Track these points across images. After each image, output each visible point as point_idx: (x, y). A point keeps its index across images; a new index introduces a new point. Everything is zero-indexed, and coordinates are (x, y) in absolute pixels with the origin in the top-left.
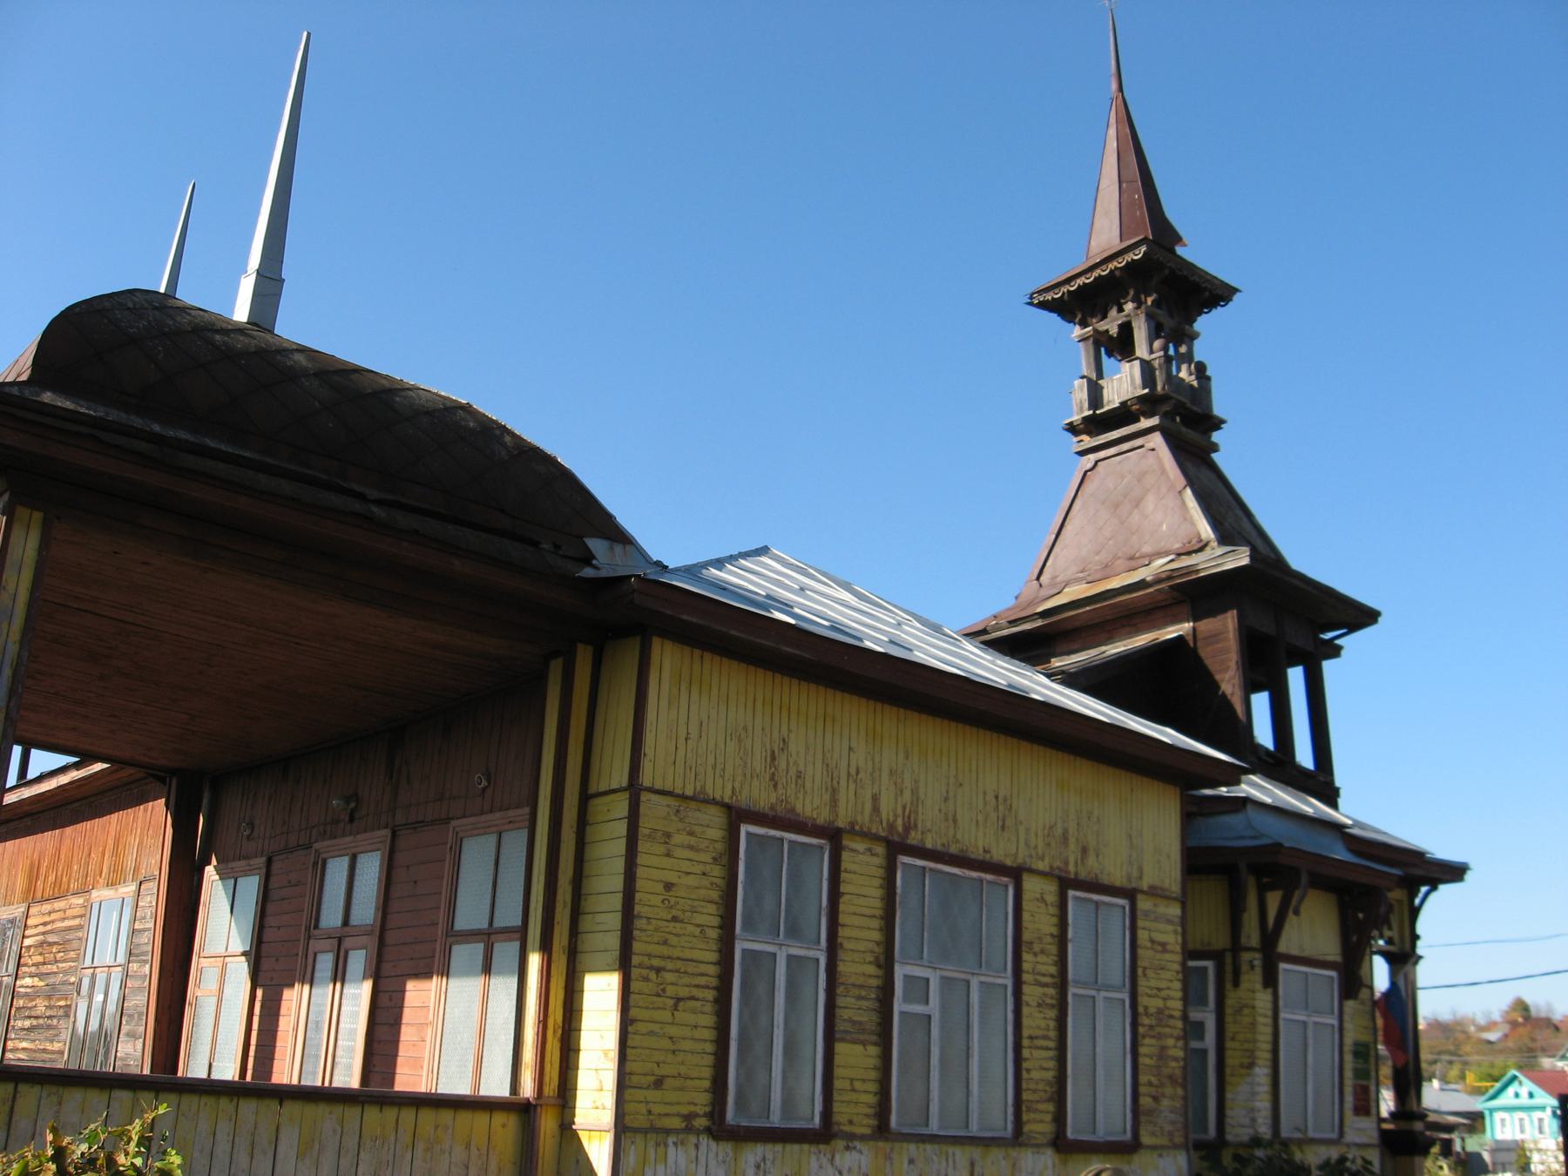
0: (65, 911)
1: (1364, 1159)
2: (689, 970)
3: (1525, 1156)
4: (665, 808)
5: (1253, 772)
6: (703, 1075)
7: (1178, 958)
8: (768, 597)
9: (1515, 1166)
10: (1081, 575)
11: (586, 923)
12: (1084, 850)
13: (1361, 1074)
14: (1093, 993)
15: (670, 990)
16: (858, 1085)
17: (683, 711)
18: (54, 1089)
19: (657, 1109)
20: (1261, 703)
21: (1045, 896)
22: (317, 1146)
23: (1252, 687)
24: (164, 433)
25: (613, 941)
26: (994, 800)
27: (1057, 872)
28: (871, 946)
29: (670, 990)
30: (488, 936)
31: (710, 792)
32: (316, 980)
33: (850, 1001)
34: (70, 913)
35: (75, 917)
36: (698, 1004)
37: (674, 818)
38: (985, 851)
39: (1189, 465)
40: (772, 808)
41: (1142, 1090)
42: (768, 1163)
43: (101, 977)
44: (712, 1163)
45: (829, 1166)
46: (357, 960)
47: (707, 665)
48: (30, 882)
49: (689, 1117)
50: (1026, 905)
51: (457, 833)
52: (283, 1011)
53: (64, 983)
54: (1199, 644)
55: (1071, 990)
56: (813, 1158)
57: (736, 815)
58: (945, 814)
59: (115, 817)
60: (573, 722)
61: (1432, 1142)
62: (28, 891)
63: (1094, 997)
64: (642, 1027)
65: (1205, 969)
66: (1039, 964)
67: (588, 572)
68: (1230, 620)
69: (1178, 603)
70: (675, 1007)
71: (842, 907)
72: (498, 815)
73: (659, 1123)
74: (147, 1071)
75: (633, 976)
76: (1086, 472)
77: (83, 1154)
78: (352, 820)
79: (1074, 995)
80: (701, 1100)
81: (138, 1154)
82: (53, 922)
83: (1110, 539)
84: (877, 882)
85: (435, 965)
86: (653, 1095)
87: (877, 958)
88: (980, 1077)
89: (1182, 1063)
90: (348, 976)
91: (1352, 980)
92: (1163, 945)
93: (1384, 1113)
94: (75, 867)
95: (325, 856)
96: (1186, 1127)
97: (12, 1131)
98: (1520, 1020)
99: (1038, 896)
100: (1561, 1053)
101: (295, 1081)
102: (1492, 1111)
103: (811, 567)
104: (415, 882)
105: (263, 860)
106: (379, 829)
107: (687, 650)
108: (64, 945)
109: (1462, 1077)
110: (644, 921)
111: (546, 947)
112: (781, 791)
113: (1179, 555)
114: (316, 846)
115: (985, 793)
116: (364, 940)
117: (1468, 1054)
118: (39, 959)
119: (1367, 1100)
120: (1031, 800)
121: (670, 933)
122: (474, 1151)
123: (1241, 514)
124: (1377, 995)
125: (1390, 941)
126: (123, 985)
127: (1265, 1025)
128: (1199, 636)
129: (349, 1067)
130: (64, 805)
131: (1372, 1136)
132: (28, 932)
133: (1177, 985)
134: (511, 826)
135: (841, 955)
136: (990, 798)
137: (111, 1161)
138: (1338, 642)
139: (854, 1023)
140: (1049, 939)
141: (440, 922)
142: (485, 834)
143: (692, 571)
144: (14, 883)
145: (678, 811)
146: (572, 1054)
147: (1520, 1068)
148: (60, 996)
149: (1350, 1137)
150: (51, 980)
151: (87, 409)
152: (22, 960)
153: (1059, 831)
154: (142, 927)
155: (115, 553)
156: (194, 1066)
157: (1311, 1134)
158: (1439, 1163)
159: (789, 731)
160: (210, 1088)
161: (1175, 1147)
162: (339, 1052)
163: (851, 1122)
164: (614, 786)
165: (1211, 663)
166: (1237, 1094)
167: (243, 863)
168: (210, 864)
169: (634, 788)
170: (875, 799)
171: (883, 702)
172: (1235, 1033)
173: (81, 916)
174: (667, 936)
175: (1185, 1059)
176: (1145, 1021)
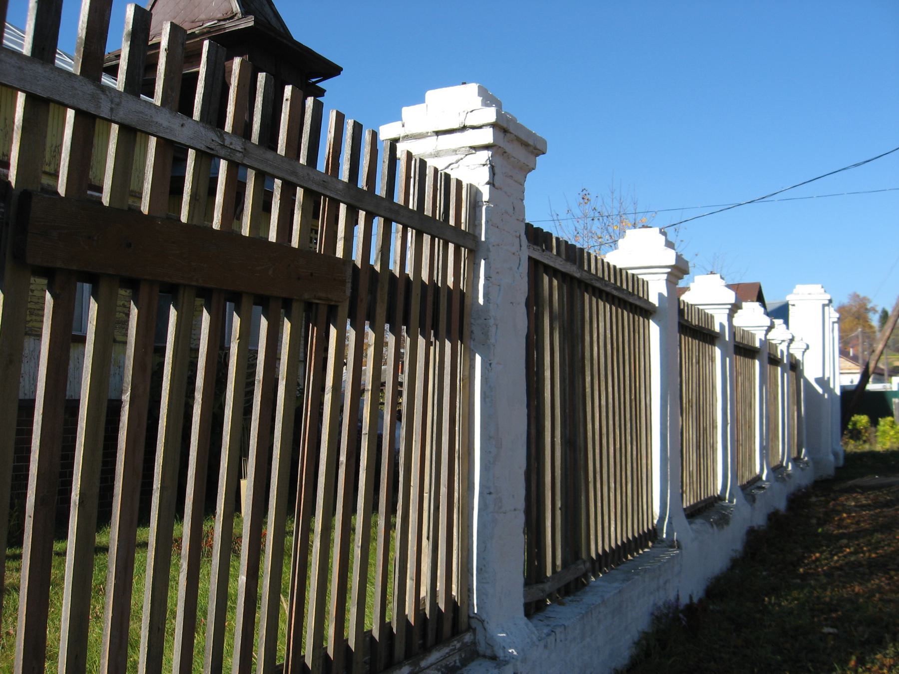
83: (182, 10)
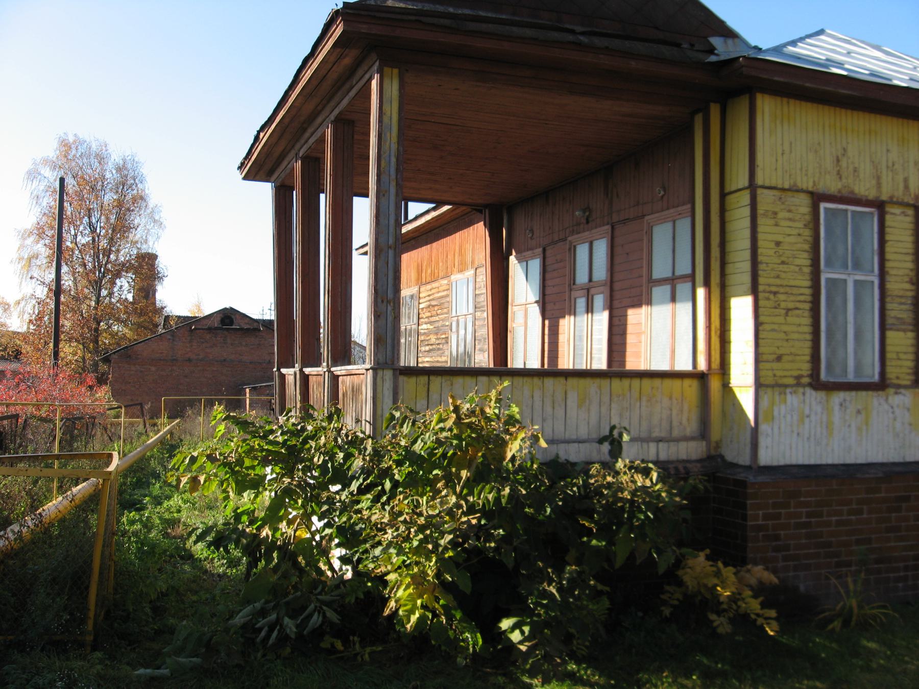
0: (438, 288)
2: (794, 292)
4: (773, 197)
8: (827, 60)
11: (730, 269)
15: (783, 305)
16: (902, 356)
18: (448, 378)
19: (779, 373)
22: (587, 401)
24: (455, 12)
25: (747, 278)
29: (783, 305)
30: (672, 281)
32: (577, 313)
33: (894, 306)
34: (441, 289)
35: (444, 291)
37: (778, 202)
40: (839, 191)
46: (599, 300)
48: (418, 275)
49: (798, 378)
51: (649, 223)
52: (561, 331)
53: (443, 326)
57: (817, 198)
59: (457, 235)
62: (418, 279)
64: (766, 327)
67: (713, 58)
70: (787, 315)
72: (672, 211)
73: (781, 381)
74: (492, 366)
77: (468, 409)
78: (588, 222)
80: (805, 368)
81: (496, 407)
85: (642, 299)
86: (775, 365)
87: (911, 279)
90: (595, 309)
94: (441, 264)
95: (574, 244)
101: (571, 367)
103: (854, 39)
104: (627, 254)
105: (541, 249)
106: (604, 226)
107: (779, 99)
110: (764, 265)
111: (707, 284)
112: (844, 181)
114: (569, 239)
116: (602, 288)
118: (429, 314)
121: (780, 271)
126: (474, 325)
129: (600, 359)
130: (430, 231)
134: (680, 216)
135: (888, 278)
137: (483, 411)
139: (898, 319)
141: (644, 274)
142: (665, 222)
143: (777, 50)
144: (410, 276)
145: (780, 198)
148: (442, 334)
150: (436, 325)
151: (412, 6)
152: (420, 316)
154: (480, 292)
155: (440, 86)
156: (516, 361)
160: (525, 373)
162: (594, 352)
164: (740, 186)
167: (530, 252)
168: (512, 255)
169: (752, 187)
170: (906, 180)
173: (447, 290)
174: (780, 273)
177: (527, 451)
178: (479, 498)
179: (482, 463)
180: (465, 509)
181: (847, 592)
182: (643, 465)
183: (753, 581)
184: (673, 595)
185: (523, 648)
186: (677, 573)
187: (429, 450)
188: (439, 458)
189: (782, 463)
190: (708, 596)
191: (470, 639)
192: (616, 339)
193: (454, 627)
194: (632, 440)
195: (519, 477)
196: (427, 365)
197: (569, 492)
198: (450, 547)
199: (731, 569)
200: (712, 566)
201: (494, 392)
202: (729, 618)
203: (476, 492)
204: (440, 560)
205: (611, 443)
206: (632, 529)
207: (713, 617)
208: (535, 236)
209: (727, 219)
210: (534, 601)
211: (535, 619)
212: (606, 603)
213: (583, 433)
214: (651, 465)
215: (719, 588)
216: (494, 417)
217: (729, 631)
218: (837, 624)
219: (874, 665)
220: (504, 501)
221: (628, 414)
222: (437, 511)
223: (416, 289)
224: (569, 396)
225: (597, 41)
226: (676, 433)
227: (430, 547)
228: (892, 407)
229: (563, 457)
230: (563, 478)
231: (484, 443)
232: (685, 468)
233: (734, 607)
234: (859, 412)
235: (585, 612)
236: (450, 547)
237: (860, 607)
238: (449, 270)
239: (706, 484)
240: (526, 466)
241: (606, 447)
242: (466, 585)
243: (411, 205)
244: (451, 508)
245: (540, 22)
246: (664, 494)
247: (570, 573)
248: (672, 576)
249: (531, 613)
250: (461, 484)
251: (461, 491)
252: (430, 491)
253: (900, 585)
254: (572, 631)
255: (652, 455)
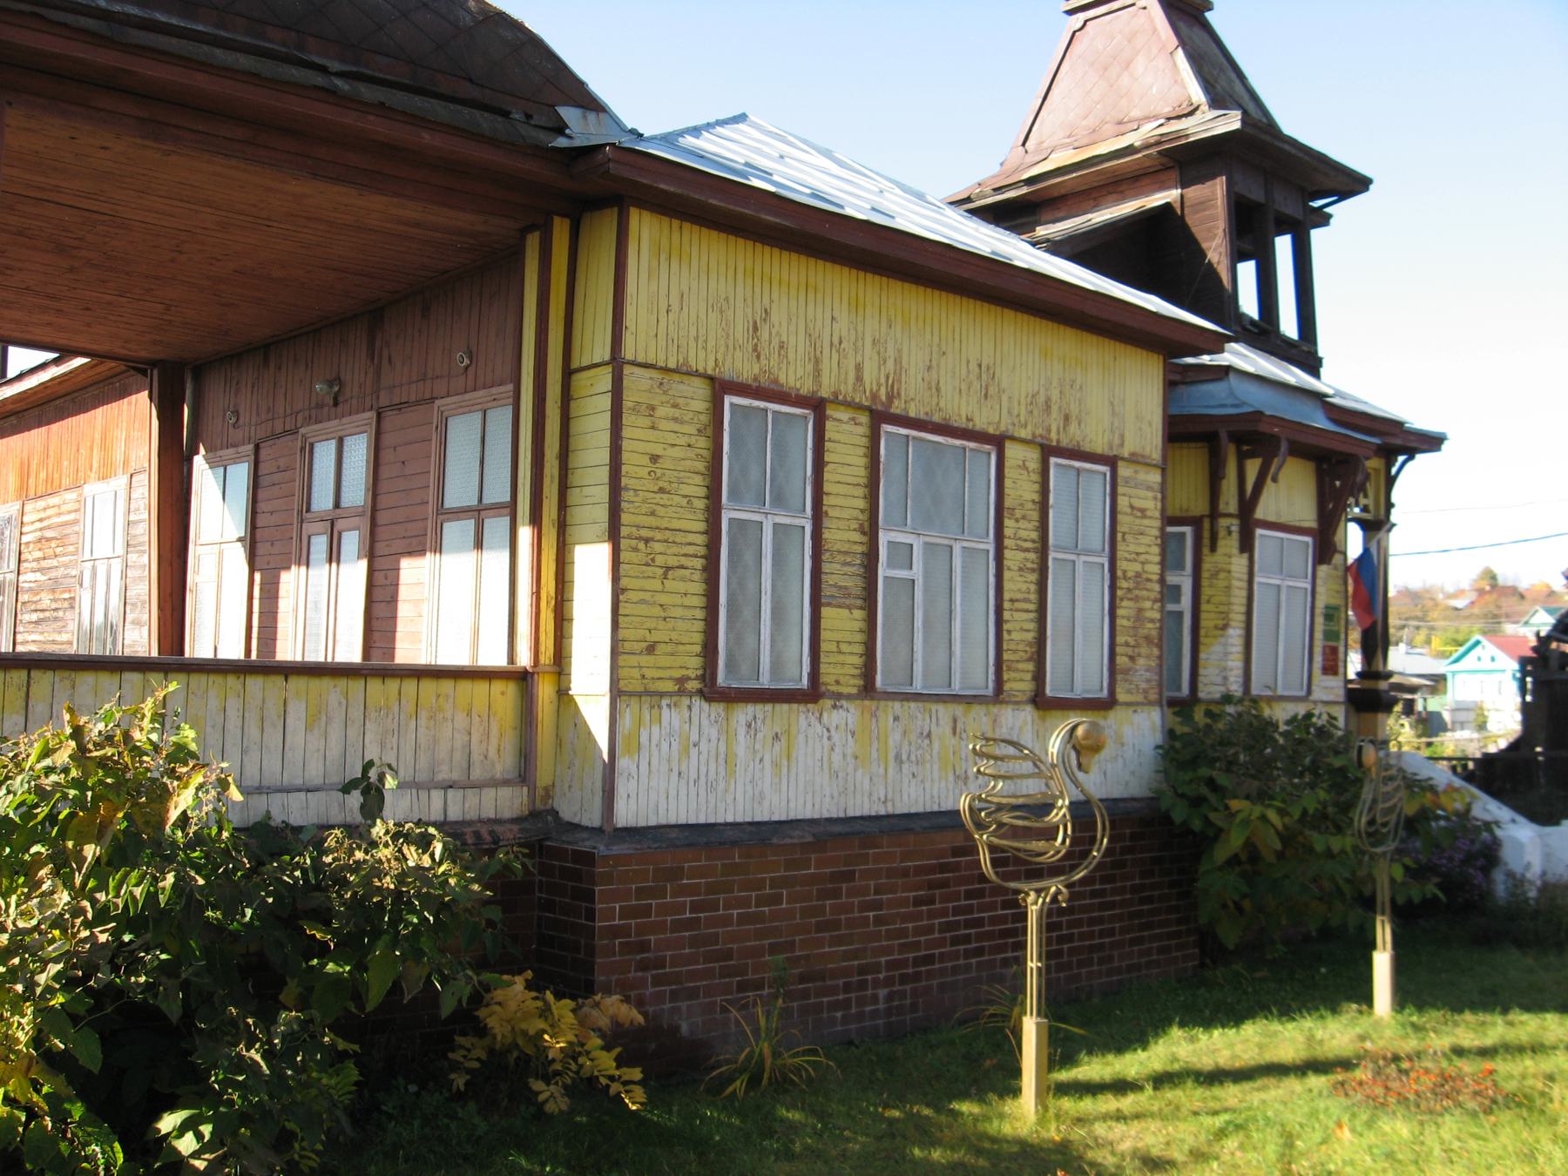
1: (1329, 714)
2: (678, 540)
3: (1483, 715)
5: (1236, 340)
6: (694, 640)
7: (1157, 523)
8: (747, 164)
9: (1473, 725)
10: (1068, 140)
11: (574, 496)
12: (1067, 418)
13: (1331, 635)
14: (1073, 557)
15: (660, 560)
16: (844, 647)
17: (664, 282)
18: (66, 674)
20: (1247, 272)
21: (1027, 464)
23: (1239, 256)
25: (602, 514)
26: (977, 369)
27: (1039, 440)
28: (856, 513)
29: (660, 560)
30: (478, 513)
31: (693, 363)
34: (65, 508)
36: (687, 572)
38: (968, 420)
39: (1181, 25)
41: (1119, 650)
42: (759, 722)
43: (101, 569)
44: (705, 722)
45: (818, 725)
46: (351, 541)
47: (686, 238)
49: (681, 681)
50: (1008, 472)
52: (282, 592)
53: (66, 576)
54: (1186, 212)
55: (1052, 555)
56: (802, 717)
57: (720, 387)
58: (929, 383)
59: (99, 411)
60: (547, 481)
61: (1395, 701)
62: (21, 488)
63: (1074, 562)
64: (632, 596)
65: (1183, 535)
66: (1021, 530)
67: (562, 142)
68: (1218, 187)
69: (1166, 169)
71: (826, 476)
72: (481, 393)
73: (652, 687)
74: (155, 653)
75: (622, 547)
76: (1074, 32)
77: (100, 732)
79: (1055, 559)
80: (694, 664)
81: (153, 730)
82: (49, 517)
84: (861, 451)
85: (426, 542)
86: (646, 660)
88: (963, 637)
89: (1158, 625)
91: (1326, 546)
92: (1142, 511)
93: (1351, 675)
94: (65, 463)
95: (311, 440)
96: (1160, 686)
97: (30, 716)
98: (1488, 588)
99: (1021, 463)
100: (1525, 619)
101: (299, 659)
102: (1454, 673)
105: (251, 447)
107: (665, 220)
108: (62, 540)
109: (1428, 642)
110: (632, 493)
111: (536, 520)
112: (764, 362)
113: (1169, 119)
114: (302, 431)
115: (968, 362)
117: (1434, 620)
118: (38, 554)
119: (1336, 660)
120: (1014, 368)
122: (476, 720)
123: (1233, 76)
124: (1350, 561)
125: (1365, 509)
126: (124, 576)
127: (1241, 589)
128: (1187, 204)
131: (1339, 695)
132: (25, 529)
133: (1156, 550)
135: (826, 522)
136: (973, 366)
137: (127, 737)
138: (1327, 210)
139: (841, 588)
140: (1030, 505)
143: (668, 139)
146: (565, 623)
147: (1484, 633)
148: (64, 592)
149: (1318, 694)
150: (53, 574)
153: (1041, 399)
156: (199, 647)
157: (1280, 692)
158: (1401, 722)
159: (771, 301)
161: (1150, 703)
163: (837, 682)
164: (597, 360)
165: (1198, 231)
166: (1210, 654)
167: (231, 451)
168: (198, 453)
169: (617, 362)
170: (859, 368)
171: (866, 271)
172: (1211, 596)
173: (76, 511)
174: (655, 507)
175: (1161, 620)
176: (1123, 584)
177: (210, 807)
178: (117, 896)
179: (124, 831)
180: (90, 916)
181: (756, 1032)
182: (418, 831)
183: (604, 1022)
184: (469, 1052)
185: (200, 1164)
186: (476, 1013)
187: (24, 809)
188: (42, 822)
189: (653, 822)
190: (530, 1051)
191: (100, 1156)
192: (380, 610)
193: (69, 1136)
194: (400, 786)
195: (196, 854)
196: (33, 648)
197: (285, 878)
198: (58, 986)
199: (568, 1003)
200: (536, 998)
201: (150, 702)
202: (565, 1087)
203: (112, 884)
204: (43, 1011)
205: (365, 793)
206: (395, 941)
207: (538, 1085)
208: (241, 422)
209: (573, 413)
210: (221, 1077)
211: (222, 1109)
212: (353, 1073)
213: (315, 773)
214: (432, 830)
215: (546, 1037)
216: (148, 747)
217: (564, 1107)
218: (739, 1085)
219: (797, 1147)
220: (162, 899)
221: (395, 740)
222: (34, 922)
223: (18, 505)
224: (290, 709)
225: (368, 92)
226: (477, 774)
227: (19, 988)
228: (828, 730)
229: (278, 818)
230: (276, 855)
231: (129, 794)
232: (491, 833)
233: (574, 1067)
234: (776, 737)
235: (314, 1092)
236: (58, 986)
237: (776, 1054)
238: (81, 474)
239: (529, 862)
240: (209, 835)
241: (355, 798)
242: (91, 1056)
243: (13, 351)
244: (61, 915)
245: (267, 45)
246: (452, 881)
247: (288, 1023)
248: (468, 1019)
249: (216, 1099)
250: (84, 870)
251: (84, 884)
252: (24, 884)
253: (839, 1014)
254: (290, 1126)
255: (436, 815)
